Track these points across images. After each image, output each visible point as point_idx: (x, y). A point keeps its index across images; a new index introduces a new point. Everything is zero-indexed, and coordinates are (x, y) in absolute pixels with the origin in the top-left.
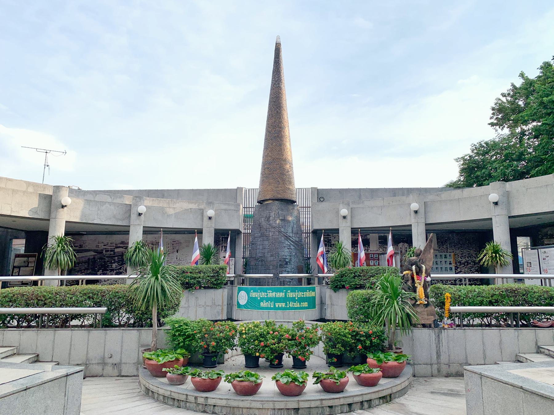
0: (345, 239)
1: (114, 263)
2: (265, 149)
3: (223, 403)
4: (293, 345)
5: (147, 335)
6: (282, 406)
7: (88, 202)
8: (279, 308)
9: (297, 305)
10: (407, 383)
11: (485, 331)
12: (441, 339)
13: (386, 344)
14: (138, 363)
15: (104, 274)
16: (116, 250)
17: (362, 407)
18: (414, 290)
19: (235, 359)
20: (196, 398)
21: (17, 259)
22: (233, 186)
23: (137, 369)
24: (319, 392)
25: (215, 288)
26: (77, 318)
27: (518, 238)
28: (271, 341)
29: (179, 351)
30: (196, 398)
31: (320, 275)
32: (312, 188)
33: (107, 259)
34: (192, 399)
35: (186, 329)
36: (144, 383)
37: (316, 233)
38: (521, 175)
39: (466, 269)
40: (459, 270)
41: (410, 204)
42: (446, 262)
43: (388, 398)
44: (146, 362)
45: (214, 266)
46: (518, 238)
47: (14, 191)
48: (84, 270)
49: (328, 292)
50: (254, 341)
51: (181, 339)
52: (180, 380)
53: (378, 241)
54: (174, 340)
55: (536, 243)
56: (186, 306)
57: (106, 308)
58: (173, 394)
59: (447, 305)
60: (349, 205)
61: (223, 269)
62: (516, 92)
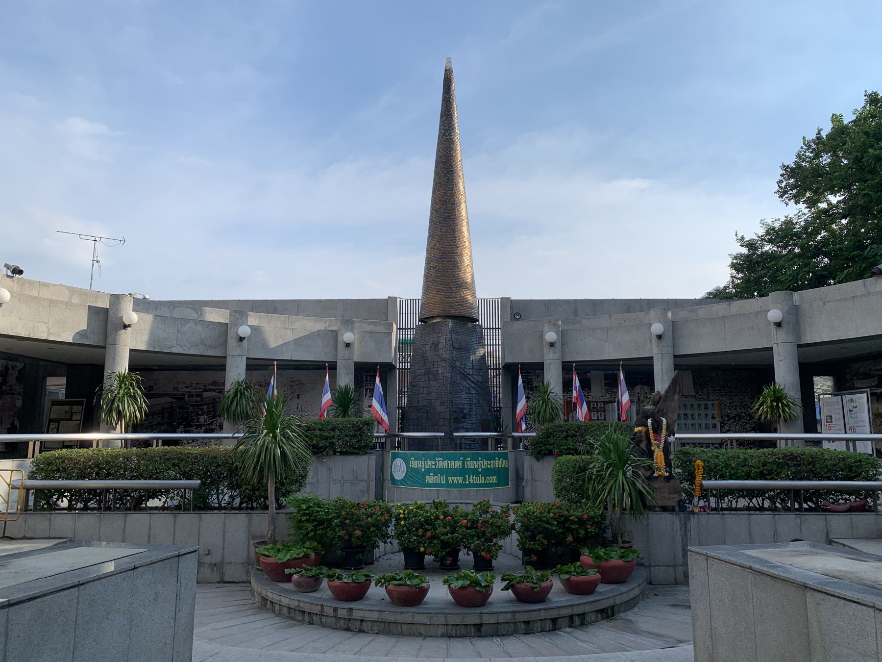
0: (553, 378)
1: (202, 415)
2: (429, 237)
3: (375, 616)
4: (473, 536)
5: (261, 522)
6: (457, 620)
8: (453, 485)
9: (481, 480)
10: (637, 591)
11: (753, 517)
13: (609, 535)
14: (248, 563)
15: (186, 432)
16: (205, 395)
17: (572, 623)
18: (650, 454)
19: (389, 555)
20: (335, 610)
21: (55, 408)
22: (382, 294)
23: (247, 572)
24: (511, 601)
25: (356, 453)
26: (157, 496)
27: (816, 379)
28: (441, 530)
29: (308, 544)
30: (335, 610)
31: (515, 434)
32: (502, 298)
33: (191, 409)
34: (329, 611)
35: (318, 512)
36: (260, 589)
37: (510, 370)
38: (820, 281)
39: (738, 427)
40: (726, 428)
41: (650, 325)
43: (610, 612)
44: (261, 559)
45: (355, 420)
46: (816, 379)
49: (528, 461)
50: (417, 530)
51: (310, 526)
52: (313, 585)
54: (300, 528)
55: (841, 387)
56: (314, 481)
57: (199, 482)
58: (301, 605)
59: (698, 478)
61: (367, 424)
62: (820, 145)
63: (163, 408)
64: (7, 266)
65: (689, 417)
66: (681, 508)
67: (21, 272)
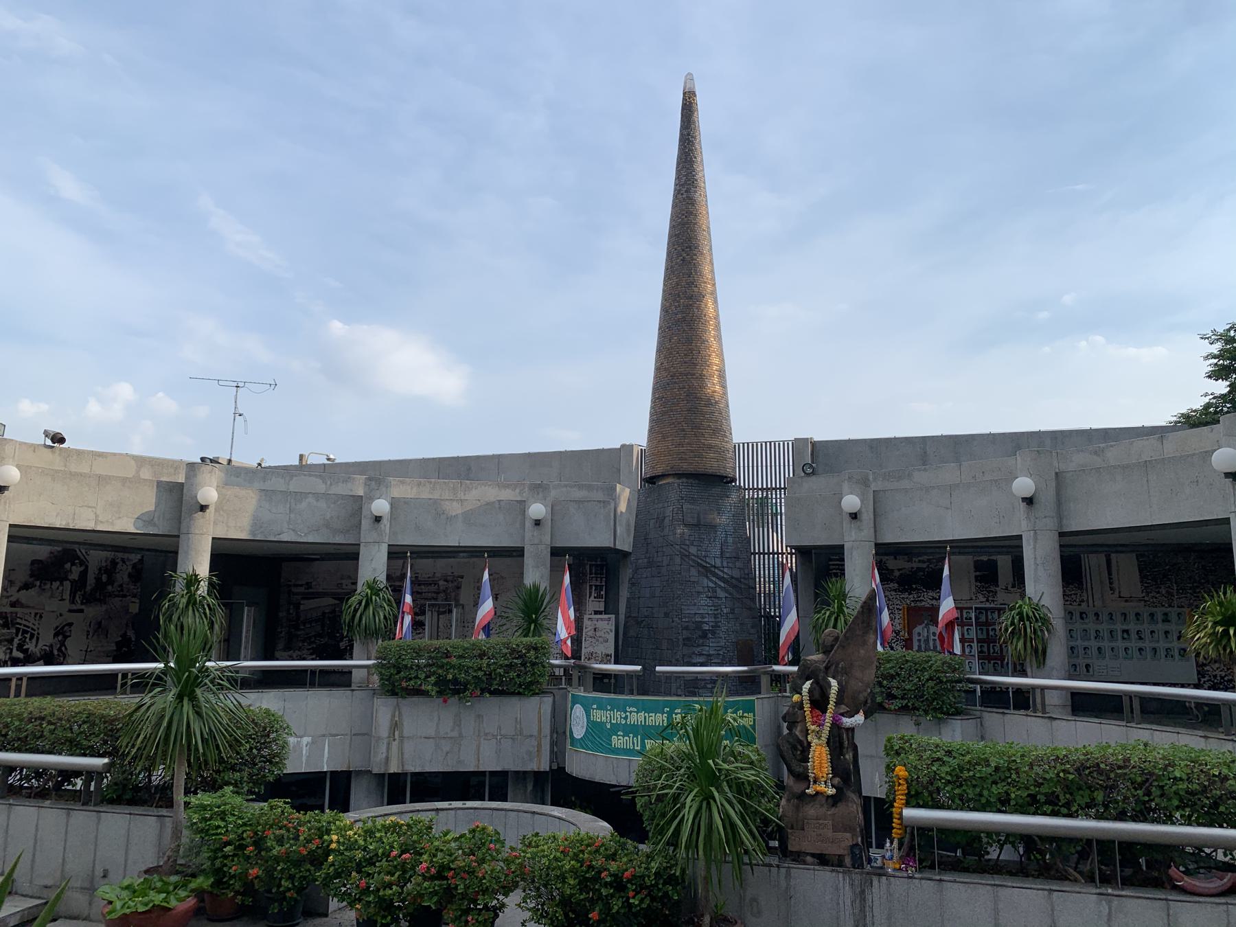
7: (267, 494)
11: (1003, 892)
12: (869, 903)
25: (519, 693)
42: (1166, 633)
47: (102, 480)
48: (315, 636)
53: (973, 574)
56: (455, 734)
63: (324, 613)
64: (46, 434)
65: (1134, 636)
66: (858, 859)
67: (62, 440)
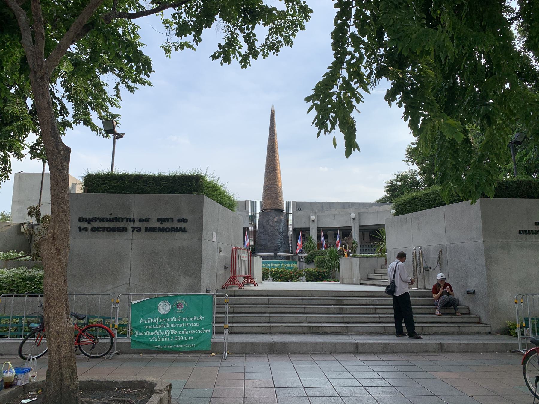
37: (296, 231)
60: (316, 213)
